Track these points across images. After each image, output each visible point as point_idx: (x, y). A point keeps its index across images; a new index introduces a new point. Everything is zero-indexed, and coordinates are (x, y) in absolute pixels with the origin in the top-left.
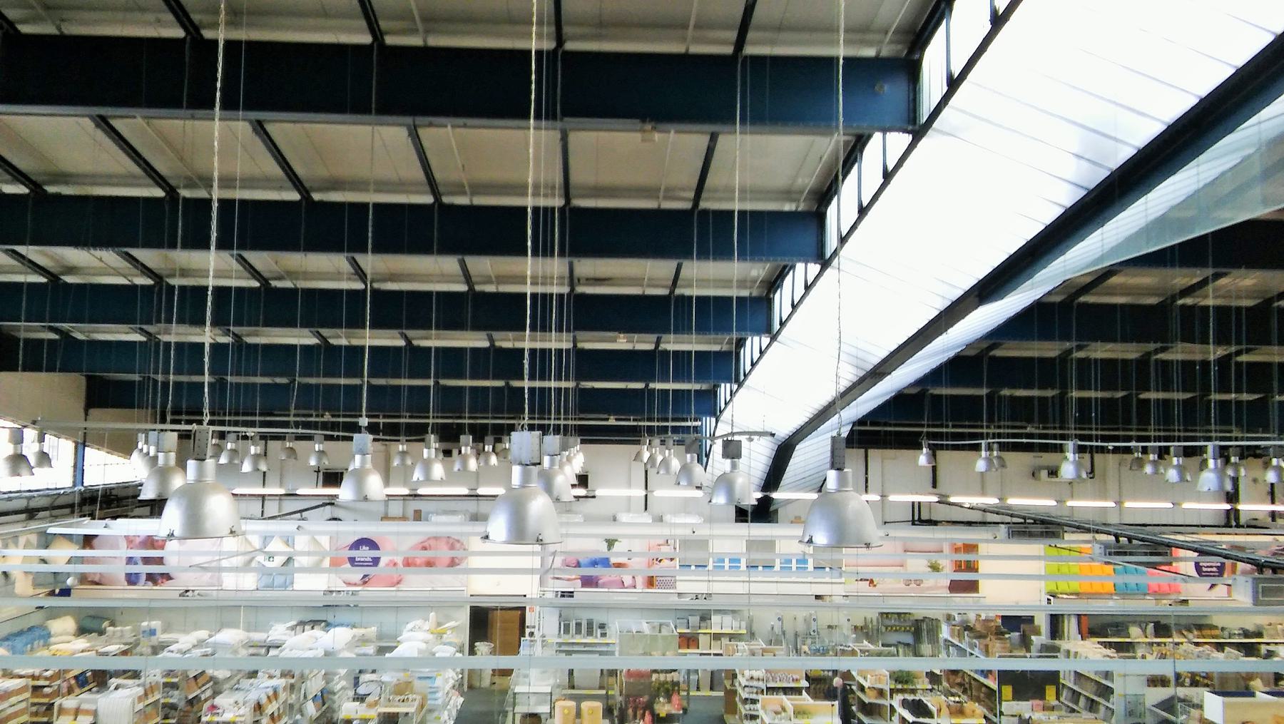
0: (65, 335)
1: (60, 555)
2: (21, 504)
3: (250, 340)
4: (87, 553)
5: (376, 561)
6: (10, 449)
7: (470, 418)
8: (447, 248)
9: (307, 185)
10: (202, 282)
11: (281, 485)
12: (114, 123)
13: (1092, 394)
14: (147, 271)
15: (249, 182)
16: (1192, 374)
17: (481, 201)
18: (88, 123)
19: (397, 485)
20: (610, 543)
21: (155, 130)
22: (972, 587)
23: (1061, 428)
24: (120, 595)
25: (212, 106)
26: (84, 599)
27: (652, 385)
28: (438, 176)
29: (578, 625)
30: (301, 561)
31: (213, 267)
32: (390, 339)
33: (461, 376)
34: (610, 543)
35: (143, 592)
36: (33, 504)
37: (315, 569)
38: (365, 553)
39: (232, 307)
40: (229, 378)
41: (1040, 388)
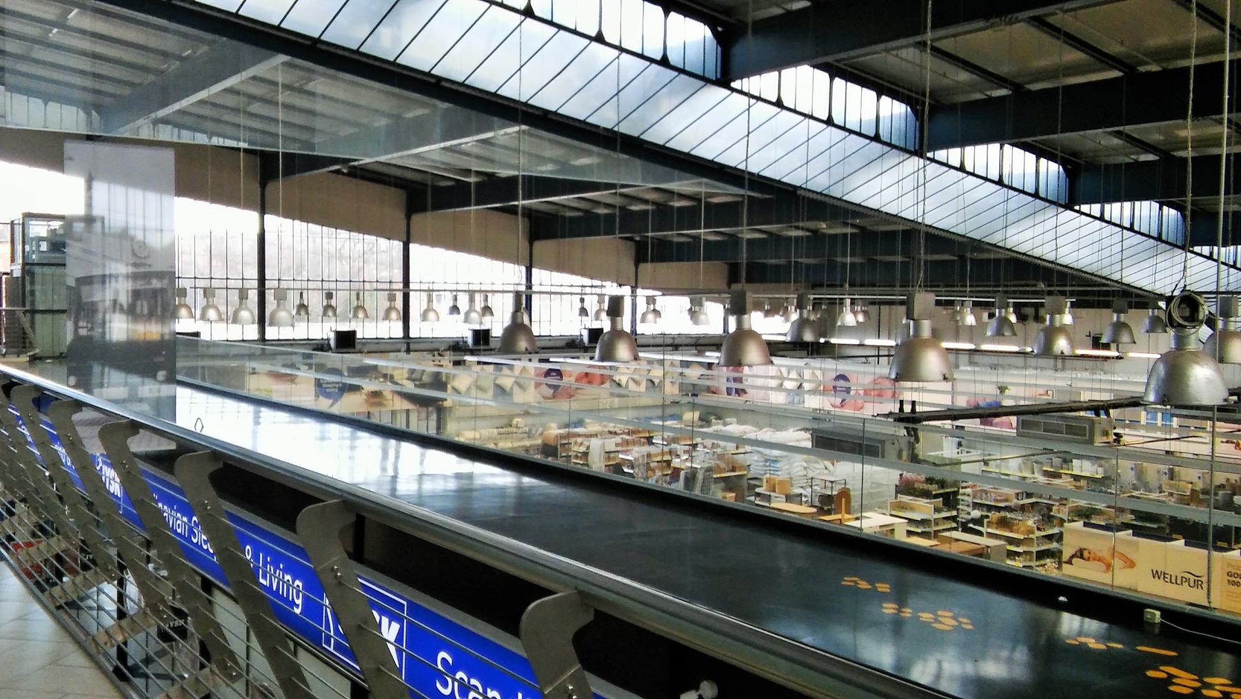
0: (815, 232)
1: (694, 374)
2: (669, 341)
4: (709, 372)
5: (848, 390)
6: (451, 304)
10: (1214, 151)
11: (971, 341)
12: (1050, 20)
19: (964, 341)
20: (1002, 389)
22: (740, 392)
24: (723, 399)
26: (704, 399)
28: (760, 103)
30: (807, 386)
34: (1002, 389)
35: (734, 399)
36: (676, 342)
37: (813, 392)
38: (842, 383)
40: (968, 255)
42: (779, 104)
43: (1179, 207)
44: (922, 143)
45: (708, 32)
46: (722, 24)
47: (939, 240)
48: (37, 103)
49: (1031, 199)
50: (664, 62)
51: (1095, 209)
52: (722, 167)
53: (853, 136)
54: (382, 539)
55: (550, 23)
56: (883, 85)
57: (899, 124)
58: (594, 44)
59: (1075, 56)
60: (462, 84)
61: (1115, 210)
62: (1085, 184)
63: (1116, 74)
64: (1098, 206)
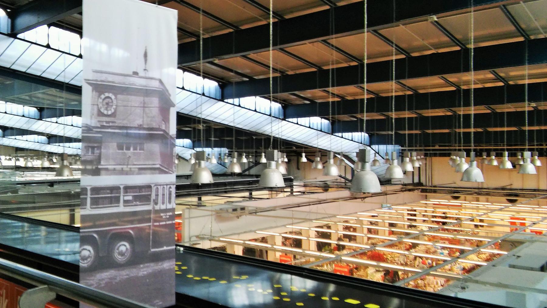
3: (498, 111)
7: (537, 145)
8: (433, 73)
9: (408, 51)
10: (390, 95)
13: (414, 132)
14: (410, 88)
15: (436, 46)
16: (516, 118)
17: (298, 72)
18: (320, 45)
21: (349, 41)
23: (459, 146)
25: (363, 27)
27: (490, 129)
29: (376, 224)
31: (473, 79)
32: (483, 110)
33: (502, 126)
39: (484, 96)
41: (537, 125)
42: (48, 46)
43: (328, 119)
44: (333, 131)
45: (280, 105)
46: (283, 103)
47: (240, 132)
48: (21, 106)
49: (181, 90)
50: (203, 94)
51: (340, 134)
52: (15, 71)
53: (33, 45)
54: (338, 215)
55: (233, 104)
56: (207, 75)
57: (326, 127)
58: (79, 59)
59: (300, 63)
60: (187, 115)
61: (346, 135)
62: (289, 111)
63: (314, 70)
64: (377, 146)
